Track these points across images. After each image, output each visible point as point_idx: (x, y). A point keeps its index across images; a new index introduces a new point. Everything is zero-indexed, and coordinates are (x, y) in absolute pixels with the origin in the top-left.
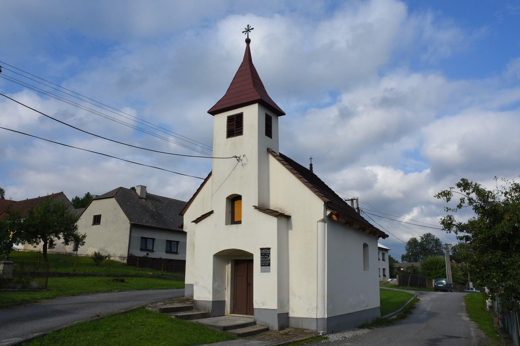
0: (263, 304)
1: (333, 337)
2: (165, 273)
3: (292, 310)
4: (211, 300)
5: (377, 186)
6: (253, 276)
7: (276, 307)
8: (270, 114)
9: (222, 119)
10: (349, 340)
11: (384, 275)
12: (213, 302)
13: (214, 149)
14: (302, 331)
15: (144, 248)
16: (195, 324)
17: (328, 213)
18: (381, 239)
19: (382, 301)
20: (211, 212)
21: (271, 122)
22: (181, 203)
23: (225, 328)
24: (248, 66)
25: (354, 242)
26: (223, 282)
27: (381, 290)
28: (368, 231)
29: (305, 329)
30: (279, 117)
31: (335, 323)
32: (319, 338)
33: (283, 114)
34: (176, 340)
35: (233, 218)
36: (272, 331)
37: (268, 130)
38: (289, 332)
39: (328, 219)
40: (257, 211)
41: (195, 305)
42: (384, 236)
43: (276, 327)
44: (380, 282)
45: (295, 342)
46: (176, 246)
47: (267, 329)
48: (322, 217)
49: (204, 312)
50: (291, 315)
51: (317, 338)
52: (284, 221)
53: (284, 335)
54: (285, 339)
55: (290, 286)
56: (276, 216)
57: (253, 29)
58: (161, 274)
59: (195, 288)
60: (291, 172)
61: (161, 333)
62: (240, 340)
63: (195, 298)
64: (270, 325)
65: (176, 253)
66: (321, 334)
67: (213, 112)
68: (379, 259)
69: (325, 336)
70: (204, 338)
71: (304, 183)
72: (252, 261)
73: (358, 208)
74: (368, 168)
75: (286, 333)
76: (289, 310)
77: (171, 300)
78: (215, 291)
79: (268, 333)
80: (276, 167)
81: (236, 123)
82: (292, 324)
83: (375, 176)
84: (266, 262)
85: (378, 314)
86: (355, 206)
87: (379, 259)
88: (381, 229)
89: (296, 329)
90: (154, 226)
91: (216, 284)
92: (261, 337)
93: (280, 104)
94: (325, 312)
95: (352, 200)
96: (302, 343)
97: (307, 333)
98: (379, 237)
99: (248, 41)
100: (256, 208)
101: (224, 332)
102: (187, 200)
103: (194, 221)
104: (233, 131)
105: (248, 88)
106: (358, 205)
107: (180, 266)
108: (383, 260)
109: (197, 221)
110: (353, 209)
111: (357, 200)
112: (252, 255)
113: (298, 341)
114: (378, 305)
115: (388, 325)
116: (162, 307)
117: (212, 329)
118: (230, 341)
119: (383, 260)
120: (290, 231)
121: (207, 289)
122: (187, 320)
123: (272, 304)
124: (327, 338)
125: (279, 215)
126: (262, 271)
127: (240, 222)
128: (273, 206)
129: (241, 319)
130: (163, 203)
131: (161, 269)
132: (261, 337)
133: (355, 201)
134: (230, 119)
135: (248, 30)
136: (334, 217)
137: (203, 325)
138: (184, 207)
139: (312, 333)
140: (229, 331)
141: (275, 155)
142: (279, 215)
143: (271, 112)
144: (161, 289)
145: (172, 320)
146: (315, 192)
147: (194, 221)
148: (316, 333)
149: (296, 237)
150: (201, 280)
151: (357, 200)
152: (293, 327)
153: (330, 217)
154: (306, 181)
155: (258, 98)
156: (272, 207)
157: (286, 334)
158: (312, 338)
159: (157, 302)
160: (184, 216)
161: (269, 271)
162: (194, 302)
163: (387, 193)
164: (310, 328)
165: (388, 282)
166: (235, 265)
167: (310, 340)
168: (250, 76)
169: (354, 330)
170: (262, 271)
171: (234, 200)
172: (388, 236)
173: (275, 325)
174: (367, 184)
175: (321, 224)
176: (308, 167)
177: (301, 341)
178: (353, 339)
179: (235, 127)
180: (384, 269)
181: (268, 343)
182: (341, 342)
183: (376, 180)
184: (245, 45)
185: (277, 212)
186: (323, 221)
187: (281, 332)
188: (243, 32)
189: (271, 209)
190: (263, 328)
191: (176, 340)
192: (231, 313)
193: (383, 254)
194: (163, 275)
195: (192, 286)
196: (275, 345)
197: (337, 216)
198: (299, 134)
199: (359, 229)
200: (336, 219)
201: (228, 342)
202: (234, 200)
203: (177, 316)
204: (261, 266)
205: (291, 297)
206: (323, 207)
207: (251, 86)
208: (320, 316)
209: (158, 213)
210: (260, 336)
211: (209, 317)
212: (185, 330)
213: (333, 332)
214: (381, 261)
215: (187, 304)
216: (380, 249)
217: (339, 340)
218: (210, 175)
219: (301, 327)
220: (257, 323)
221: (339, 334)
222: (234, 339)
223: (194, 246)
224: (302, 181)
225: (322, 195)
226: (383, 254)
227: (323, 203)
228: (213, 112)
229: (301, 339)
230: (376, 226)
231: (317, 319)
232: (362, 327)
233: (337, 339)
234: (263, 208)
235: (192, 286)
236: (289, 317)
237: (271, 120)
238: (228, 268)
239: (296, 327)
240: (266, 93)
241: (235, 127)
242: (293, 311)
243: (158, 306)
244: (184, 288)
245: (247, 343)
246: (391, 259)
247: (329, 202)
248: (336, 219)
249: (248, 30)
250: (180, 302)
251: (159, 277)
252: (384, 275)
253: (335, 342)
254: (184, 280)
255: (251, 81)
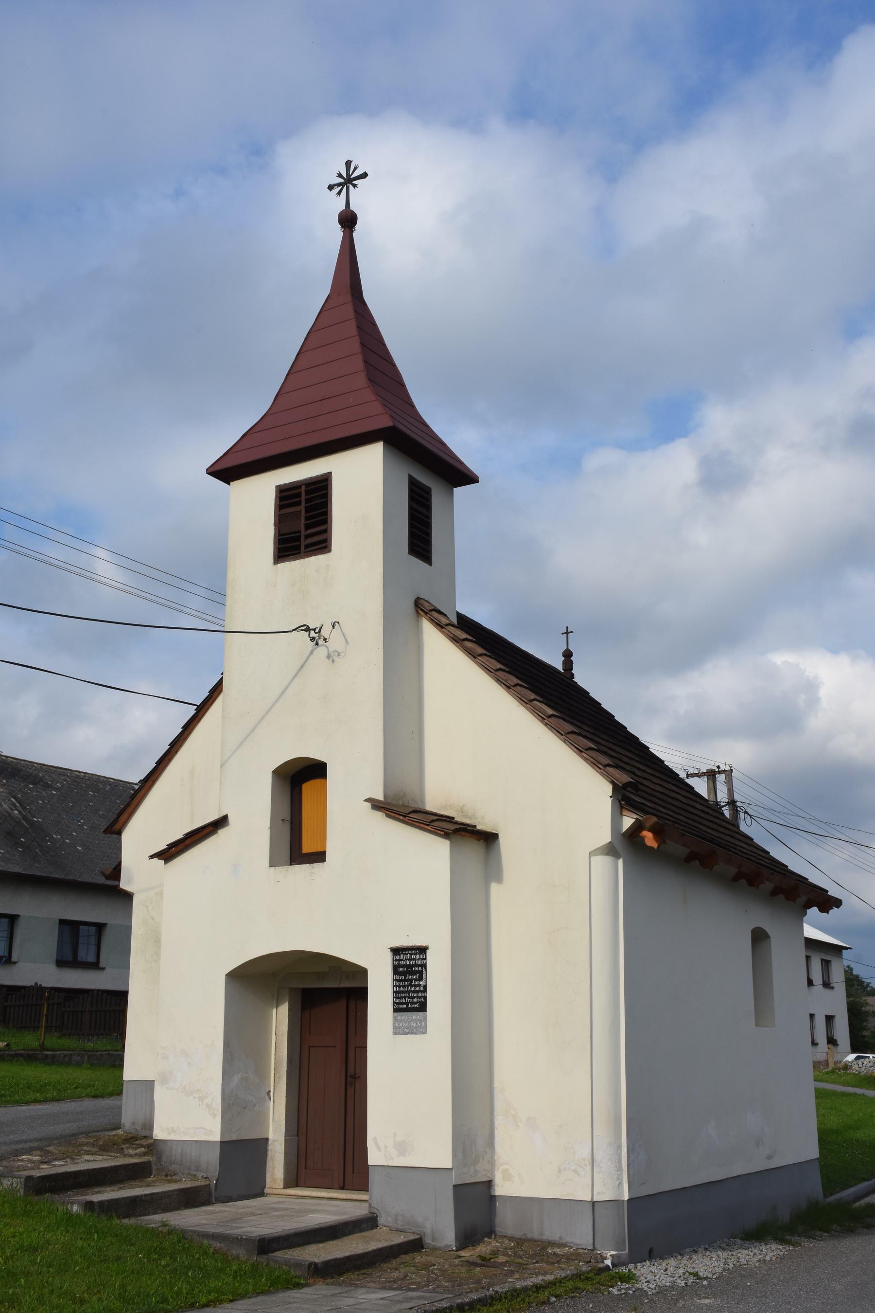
0: (402, 1148)
1: (653, 1275)
2: (53, 1041)
3: (505, 1171)
4: (218, 1138)
5: (817, 723)
6: (365, 1047)
7: (445, 1160)
8: (424, 478)
9: (259, 494)
10: (710, 1285)
11: (832, 1041)
12: (223, 1143)
13: (229, 601)
14: (540, 1250)
15: (69, 957)
16: (154, 1233)
17: (628, 822)
18: (814, 911)
19: (825, 1138)
20: (221, 823)
21: (429, 508)
22: (115, 786)
23: (266, 1245)
24: (348, 311)
25: (720, 924)
26: (261, 1071)
27: (820, 1095)
28: (768, 886)
29: (551, 1244)
30: (457, 490)
31: (659, 1220)
32: (603, 1276)
33: (466, 478)
34: (82, 1302)
35: (297, 842)
36: (435, 1249)
37: (419, 535)
38: (495, 1253)
39: (628, 844)
40: (379, 815)
41: (159, 1159)
42: (826, 902)
43: (448, 1236)
44: (816, 1065)
45: (515, 1293)
46: (93, 940)
47: (416, 1245)
48: (605, 836)
49: (189, 1185)
50: (501, 1189)
51: (594, 1277)
52: (473, 850)
53: (475, 1264)
54: (478, 1282)
55: (496, 1084)
56: (446, 835)
57: (364, 175)
58: (36, 1044)
59: (160, 1095)
60: (499, 681)
61: (27, 1274)
62: (319, 1290)
63: (159, 1133)
64: (428, 1231)
65: (95, 966)
66: (608, 1262)
67: (228, 471)
68: (810, 983)
69: (624, 1270)
70: (185, 1288)
71: (544, 719)
72: (361, 994)
73: (732, 803)
74: (780, 659)
75: (483, 1259)
76: (493, 1174)
77: (71, 1143)
78: (237, 1102)
79: (419, 1258)
80: (445, 663)
81: (308, 510)
82: (507, 1222)
83: (811, 687)
84: (410, 999)
85: (814, 1186)
86: (722, 796)
87: (810, 983)
88: (815, 878)
89: (520, 1242)
90: (15, 869)
91: (236, 1079)
92: (396, 1274)
93: (461, 439)
94: (620, 1178)
95: (711, 775)
96: (543, 1295)
97: (557, 1259)
98: (808, 906)
99: (348, 220)
100: (376, 805)
101: (263, 1259)
102: (135, 776)
103: (159, 855)
104: (298, 539)
105: (346, 400)
106: (731, 791)
107: (107, 1014)
108: (827, 985)
109: (169, 854)
110: (716, 807)
111: (729, 773)
112: (362, 973)
113: (525, 1289)
114: (812, 1151)
115: (850, 1231)
116: (36, 1173)
117: (216, 1251)
118: (281, 1295)
119: (827, 985)
120: (494, 887)
121: (201, 1099)
122: (127, 1216)
123: (435, 1151)
124: (628, 1278)
125: (456, 831)
126: (397, 1031)
127: (319, 857)
128: (434, 801)
129: (325, 1206)
130: (47, 786)
131: (36, 1028)
132: (396, 1274)
133: (721, 778)
134: (286, 496)
135: (349, 180)
136: (648, 837)
137: (183, 1236)
138: (126, 799)
139: (575, 1256)
140: (279, 1254)
141: (444, 621)
142: (456, 831)
143: (430, 472)
144: (36, 1101)
145: (70, 1219)
146: (580, 751)
147: (159, 855)
148: (592, 1256)
149: (514, 904)
150: (183, 1068)
151: (729, 773)
152: (510, 1232)
153: (632, 837)
154: (550, 712)
155: (385, 422)
156: (433, 803)
157: (484, 1261)
158: (578, 1276)
159: (17, 1153)
160: (123, 835)
161: (422, 1029)
162: (154, 1147)
163: (851, 747)
164: (568, 1239)
165: (846, 1067)
166: (304, 1008)
167: (571, 1284)
168: (354, 345)
169: (727, 1247)
170: (397, 1031)
171: (300, 779)
172: (838, 903)
173: (442, 1227)
174: (778, 717)
175: (602, 863)
176: (558, 663)
177: (538, 1288)
178: (726, 1284)
179: (303, 525)
180: (829, 1019)
181: (421, 1298)
182: (683, 1292)
183: (814, 701)
184: (338, 233)
185: (450, 819)
186: (610, 850)
187: (466, 1254)
188: (331, 187)
189: (429, 807)
190: (400, 1239)
191: (82, 1302)
192: (286, 1186)
193: (826, 964)
194: (43, 1047)
195: (148, 1086)
196: (445, 1304)
197: (657, 832)
198: (521, 547)
199: (736, 879)
200: (655, 845)
201: (273, 1298)
202: (300, 779)
203: (89, 1206)
204: (395, 1010)
205: (499, 1121)
206: (610, 800)
207: (361, 380)
208: (604, 1194)
209: (32, 824)
210: (392, 1271)
211: (207, 1202)
212: (118, 1259)
213: (651, 1255)
214: (818, 988)
215: (131, 1157)
216: (811, 944)
217: (673, 1286)
218: (216, 690)
219: (536, 1236)
220: (381, 1220)
221: (672, 1262)
222: (298, 1286)
223: (158, 941)
224: (536, 712)
225: (605, 760)
226: (826, 964)
227: (608, 789)
228: (228, 471)
229: (538, 1280)
230: (796, 865)
231: (594, 1203)
232: (757, 1234)
233: (666, 1281)
234: (402, 808)
235: (148, 1086)
236: (493, 1198)
237: (429, 500)
238: (280, 1017)
239: (518, 1234)
240: (412, 406)
241: (303, 525)
242: (508, 1177)
243: (20, 1169)
244: (120, 1093)
245: (346, 1302)
246: (853, 983)
247: (626, 785)
248: (655, 845)
249: (349, 180)
250: (104, 1149)
251: (30, 1057)
252: (832, 1041)
253: (662, 1291)
254: (121, 1066)
255: (358, 363)
